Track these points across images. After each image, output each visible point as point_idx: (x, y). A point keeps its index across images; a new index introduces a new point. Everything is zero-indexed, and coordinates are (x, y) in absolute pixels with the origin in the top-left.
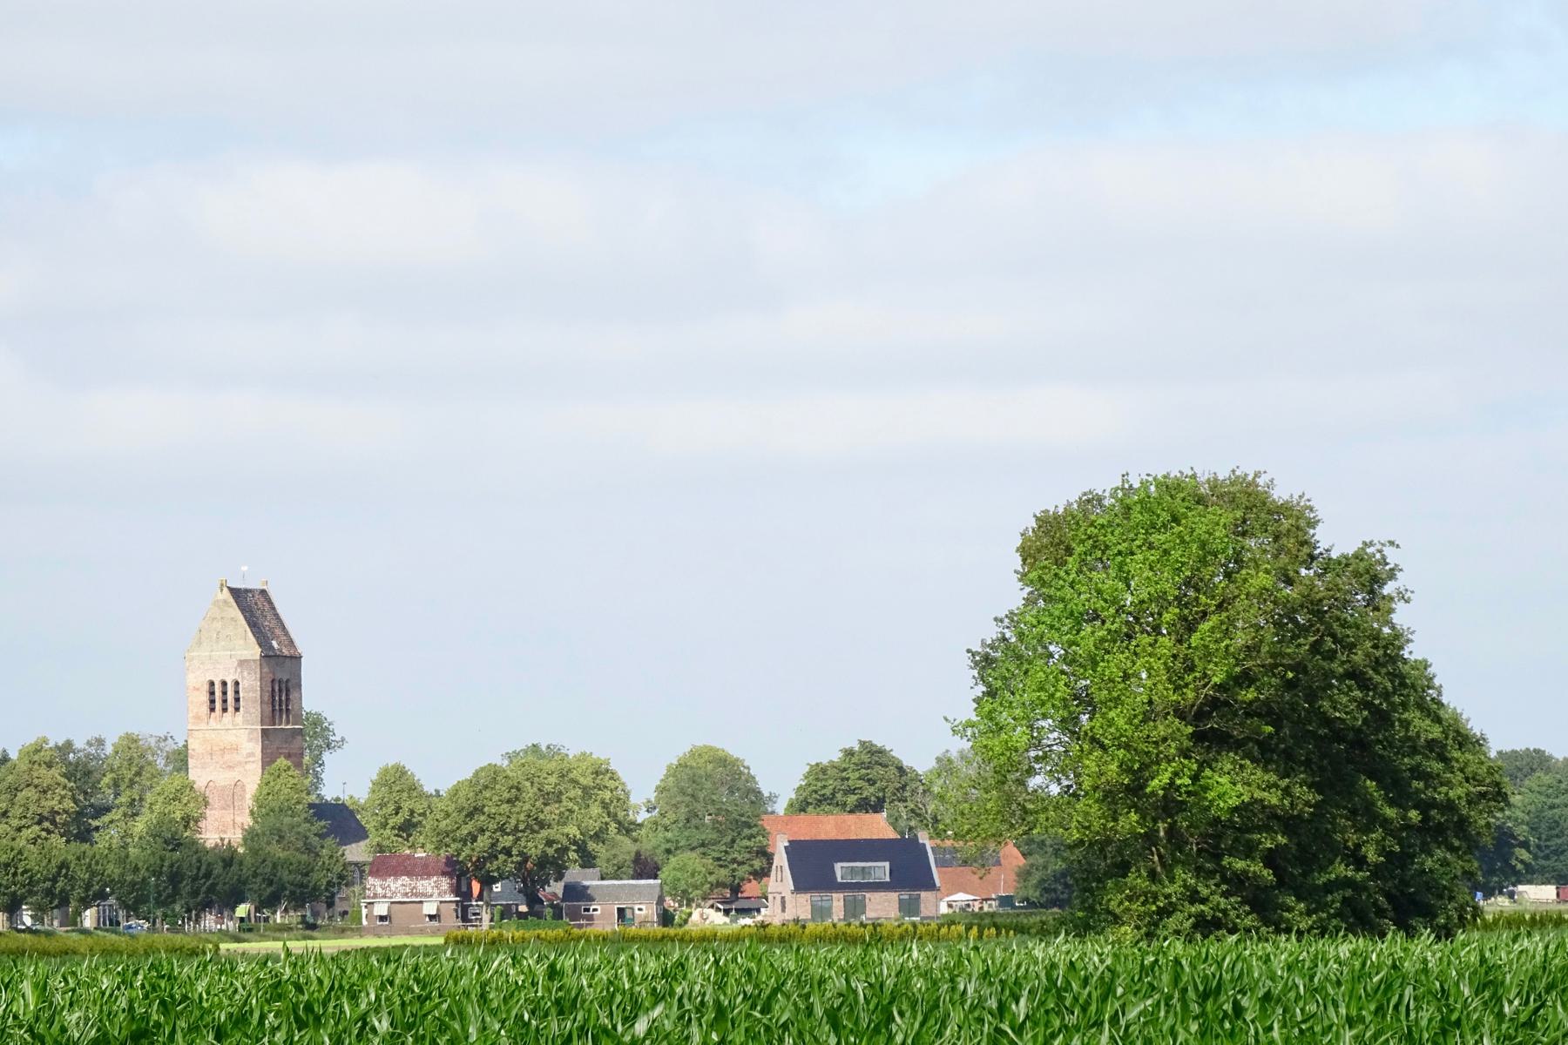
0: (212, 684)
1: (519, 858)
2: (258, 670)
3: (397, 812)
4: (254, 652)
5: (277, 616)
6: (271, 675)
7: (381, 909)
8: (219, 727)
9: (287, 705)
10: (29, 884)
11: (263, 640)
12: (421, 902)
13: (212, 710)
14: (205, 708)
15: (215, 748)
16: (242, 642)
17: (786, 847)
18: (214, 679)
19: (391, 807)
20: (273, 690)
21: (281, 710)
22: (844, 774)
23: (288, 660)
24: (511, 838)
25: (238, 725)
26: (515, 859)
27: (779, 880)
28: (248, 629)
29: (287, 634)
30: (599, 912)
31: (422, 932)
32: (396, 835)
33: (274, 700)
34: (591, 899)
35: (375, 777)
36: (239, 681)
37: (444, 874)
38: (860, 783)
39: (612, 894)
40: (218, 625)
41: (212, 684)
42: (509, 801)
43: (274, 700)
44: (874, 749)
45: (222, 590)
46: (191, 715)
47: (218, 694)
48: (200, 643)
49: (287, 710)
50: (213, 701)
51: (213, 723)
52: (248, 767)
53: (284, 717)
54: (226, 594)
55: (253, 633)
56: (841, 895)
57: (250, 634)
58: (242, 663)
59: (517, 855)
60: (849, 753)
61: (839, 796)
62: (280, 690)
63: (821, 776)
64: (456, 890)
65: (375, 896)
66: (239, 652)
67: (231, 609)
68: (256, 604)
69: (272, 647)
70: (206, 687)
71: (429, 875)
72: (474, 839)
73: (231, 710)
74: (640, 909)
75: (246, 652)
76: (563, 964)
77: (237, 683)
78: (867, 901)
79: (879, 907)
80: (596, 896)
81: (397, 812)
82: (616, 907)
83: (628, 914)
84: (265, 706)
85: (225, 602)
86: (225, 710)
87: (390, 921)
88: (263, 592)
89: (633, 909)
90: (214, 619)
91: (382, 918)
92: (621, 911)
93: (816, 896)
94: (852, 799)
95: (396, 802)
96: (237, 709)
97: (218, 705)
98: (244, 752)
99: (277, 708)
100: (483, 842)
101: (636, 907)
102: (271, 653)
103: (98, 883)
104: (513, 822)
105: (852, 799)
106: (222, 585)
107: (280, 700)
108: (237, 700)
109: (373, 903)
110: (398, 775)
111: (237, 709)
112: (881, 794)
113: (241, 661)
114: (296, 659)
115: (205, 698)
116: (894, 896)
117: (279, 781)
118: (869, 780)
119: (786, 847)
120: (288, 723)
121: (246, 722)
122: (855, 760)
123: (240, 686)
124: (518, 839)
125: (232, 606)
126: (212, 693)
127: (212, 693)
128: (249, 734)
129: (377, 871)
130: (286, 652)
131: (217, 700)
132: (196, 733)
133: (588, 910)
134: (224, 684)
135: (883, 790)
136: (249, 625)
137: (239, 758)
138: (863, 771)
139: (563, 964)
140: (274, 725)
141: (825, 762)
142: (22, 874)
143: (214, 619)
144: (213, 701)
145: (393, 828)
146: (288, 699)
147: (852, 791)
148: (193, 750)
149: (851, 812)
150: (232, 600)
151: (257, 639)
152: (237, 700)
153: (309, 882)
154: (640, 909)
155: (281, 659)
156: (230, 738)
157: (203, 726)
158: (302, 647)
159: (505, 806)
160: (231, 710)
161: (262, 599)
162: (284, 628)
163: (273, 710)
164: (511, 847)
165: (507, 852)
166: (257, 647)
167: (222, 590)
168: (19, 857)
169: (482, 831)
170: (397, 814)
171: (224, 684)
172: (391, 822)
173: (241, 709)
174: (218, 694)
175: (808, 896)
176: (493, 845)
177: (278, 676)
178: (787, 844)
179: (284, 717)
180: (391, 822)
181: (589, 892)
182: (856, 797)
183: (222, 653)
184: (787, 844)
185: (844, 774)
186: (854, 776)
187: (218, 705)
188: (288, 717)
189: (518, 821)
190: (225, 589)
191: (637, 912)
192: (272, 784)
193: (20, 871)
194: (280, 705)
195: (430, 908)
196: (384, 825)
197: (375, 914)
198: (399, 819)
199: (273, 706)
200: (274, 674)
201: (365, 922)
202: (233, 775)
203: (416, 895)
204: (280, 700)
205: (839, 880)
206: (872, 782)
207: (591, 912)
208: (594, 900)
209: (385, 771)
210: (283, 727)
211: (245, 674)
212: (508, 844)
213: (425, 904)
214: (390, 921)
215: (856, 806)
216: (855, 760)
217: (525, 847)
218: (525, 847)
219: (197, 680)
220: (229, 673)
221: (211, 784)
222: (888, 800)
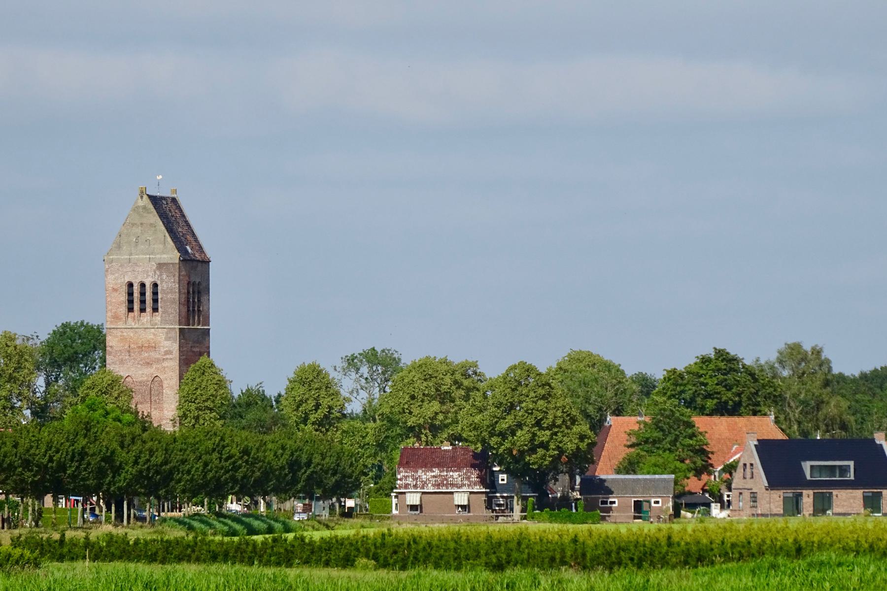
0: (130, 285)
1: (556, 452)
2: (177, 274)
3: (317, 406)
4: (173, 256)
5: (187, 222)
6: (187, 278)
7: (413, 499)
8: (137, 326)
9: (199, 307)
10: (232, 470)
11: (181, 248)
12: (452, 493)
13: (131, 309)
14: (123, 309)
15: (132, 346)
16: (161, 246)
17: (756, 446)
18: (133, 281)
19: (311, 403)
20: (188, 292)
21: (194, 310)
22: (702, 379)
23: (200, 264)
24: (548, 433)
25: (156, 324)
26: (551, 452)
27: (748, 475)
28: (167, 234)
29: (196, 240)
30: (616, 505)
31: (453, 520)
32: (316, 430)
33: (188, 301)
34: (610, 492)
35: (292, 376)
36: (159, 283)
37: (473, 466)
38: (720, 388)
39: (626, 487)
40: (138, 230)
41: (130, 285)
42: (543, 398)
43: (188, 301)
44: (730, 357)
45: (142, 197)
46: (109, 314)
47: (136, 295)
48: (119, 246)
49: (199, 311)
50: (131, 302)
51: (131, 323)
52: (165, 364)
53: (196, 318)
54: (146, 201)
55: (171, 238)
56: (811, 492)
57: (169, 239)
58: (161, 266)
59: (553, 450)
60: (705, 360)
61: (699, 400)
62: (194, 292)
63: (680, 381)
64: (483, 482)
65: (406, 486)
66: (158, 256)
67: (151, 215)
68: (170, 211)
69: (187, 251)
70: (124, 289)
71: (459, 468)
72: (513, 434)
73: (149, 309)
74: (657, 502)
75: (165, 256)
76: (871, 556)
77: (155, 285)
78: (834, 497)
79: (845, 503)
80: (613, 489)
81: (317, 406)
82: (633, 500)
83: (645, 506)
84: (182, 307)
85: (144, 208)
86: (143, 310)
87: (421, 512)
88: (174, 200)
89: (649, 502)
90: (133, 225)
91: (413, 508)
92: (638, 506)
93: (789, 493)
94: (710, 404)
95: (315, 399)
96: (155, 310)
97: (136, 306)
98: (163, 350)
99: (191, 309)
100: (522, 436)
101: (653, 500)
102: (187, 257)
103: (259, 470)
104: (550, 417)
105: (710, 404)
106: (142, 192)
107: (194, 301)
108: (155, 301)
109: (404, 493)
110: (315, 374)
111: (155, 310)
112: (737, 399)
113: (159, 264)
114: (207, 262)
115: (124, 297)
116: (859, 493)
117: (205, 378)
118: (725, 386)
119: (756, 446)
120: (198, 325)
121: (164, 321)
122: (712, 366)
123: (159, 288)
124: (556, 434)
125: (151, 213)
126: (130, 294)
127: (130, 294)
128: (167, 333)
129: (407, 463)
130: (199, 258)
131: (147, 302)
132: (115, 331)
133: (606, 503)
134: (143, 285)
135: (739, 395)
136: (167, 231)
137: (154, 355)
138: (721, 377)
139: (871, 556)
140: (189, 325)
141: (681, 368)
142: (227, 460)
143: (133, 225)
144: (131, 302)
145: (313, 424)
146: (199, 301)
147: (709, 396)
148: (111, 347)
149: (710, 414)
150: (151, 206)
151: (175, 242)
152: (155, 301)
153: (353, 472)
154: (657, 502)
155: (195, 264)
156: (149, 336)
157: (121, 325)
158: (209, 252)
159: (541, 402)
160: (149, 309)
161: (174, 207)
162: (194, 235)
163: (188, 311)
164: (548, 442)
165: (544, 446)
166: (176, 251)
167: (142, 197)
168: (222, 443)
169: (520, 426)
170: (316, 410)
171: (143, 285)
172: (312, 418)
173: (160, 309)
174: (136, 295)
175: (781, 493)
176: (532, 440)
177: (193, 279)
178: (756, 443)
179: (196, 318)
180: (312, 418)
181: (606, 484)
182: (715, 401)
183: (141, 256)
184: (756, 443)
185: (702, 379)
186: (712, 382)
187: (136, 306)
188: (199, 317)
189: (555, 417)
190: (145, 197)
191: (653, 505)
192: (198, 380)
193: (224, 457)
194: (194, 307)
195: (461, 499)
196: (305, 421)
197: (408, 503)
198: (320, 414)
199: (188, 307)
200: (189, 278)
201: (395, 512)
202: (152, 371)
203: (447, 486)
204: (194, 301)
205: (808, 477)
206: (729, 388)
207: (609, 505)
208: (612, 493)
209: (303, 370)
210: (195, 327)
211: (164, 277)
212: (545, 439)
213: (408, 495)
214: (421, 512)
215: (713, 410)
216: (712, 366)
217: (560, 442)
218: (560, 442)
219: (117, 280)
220: (148, 276)
221: (156, 379)
222: (744, 405)
